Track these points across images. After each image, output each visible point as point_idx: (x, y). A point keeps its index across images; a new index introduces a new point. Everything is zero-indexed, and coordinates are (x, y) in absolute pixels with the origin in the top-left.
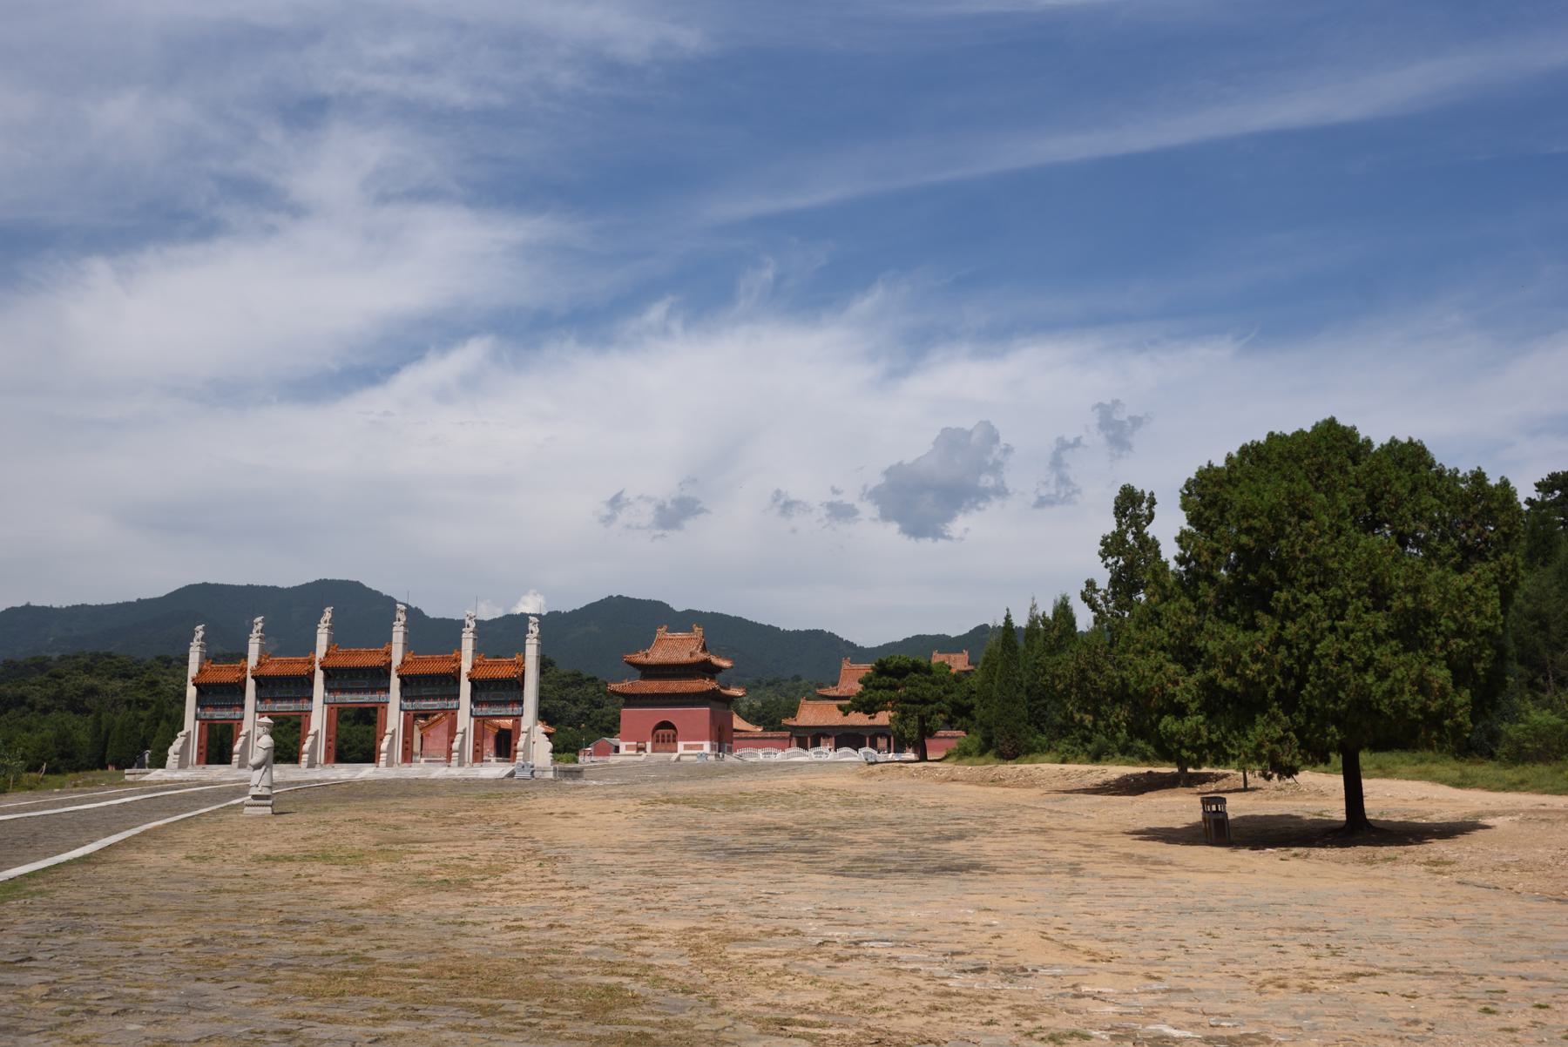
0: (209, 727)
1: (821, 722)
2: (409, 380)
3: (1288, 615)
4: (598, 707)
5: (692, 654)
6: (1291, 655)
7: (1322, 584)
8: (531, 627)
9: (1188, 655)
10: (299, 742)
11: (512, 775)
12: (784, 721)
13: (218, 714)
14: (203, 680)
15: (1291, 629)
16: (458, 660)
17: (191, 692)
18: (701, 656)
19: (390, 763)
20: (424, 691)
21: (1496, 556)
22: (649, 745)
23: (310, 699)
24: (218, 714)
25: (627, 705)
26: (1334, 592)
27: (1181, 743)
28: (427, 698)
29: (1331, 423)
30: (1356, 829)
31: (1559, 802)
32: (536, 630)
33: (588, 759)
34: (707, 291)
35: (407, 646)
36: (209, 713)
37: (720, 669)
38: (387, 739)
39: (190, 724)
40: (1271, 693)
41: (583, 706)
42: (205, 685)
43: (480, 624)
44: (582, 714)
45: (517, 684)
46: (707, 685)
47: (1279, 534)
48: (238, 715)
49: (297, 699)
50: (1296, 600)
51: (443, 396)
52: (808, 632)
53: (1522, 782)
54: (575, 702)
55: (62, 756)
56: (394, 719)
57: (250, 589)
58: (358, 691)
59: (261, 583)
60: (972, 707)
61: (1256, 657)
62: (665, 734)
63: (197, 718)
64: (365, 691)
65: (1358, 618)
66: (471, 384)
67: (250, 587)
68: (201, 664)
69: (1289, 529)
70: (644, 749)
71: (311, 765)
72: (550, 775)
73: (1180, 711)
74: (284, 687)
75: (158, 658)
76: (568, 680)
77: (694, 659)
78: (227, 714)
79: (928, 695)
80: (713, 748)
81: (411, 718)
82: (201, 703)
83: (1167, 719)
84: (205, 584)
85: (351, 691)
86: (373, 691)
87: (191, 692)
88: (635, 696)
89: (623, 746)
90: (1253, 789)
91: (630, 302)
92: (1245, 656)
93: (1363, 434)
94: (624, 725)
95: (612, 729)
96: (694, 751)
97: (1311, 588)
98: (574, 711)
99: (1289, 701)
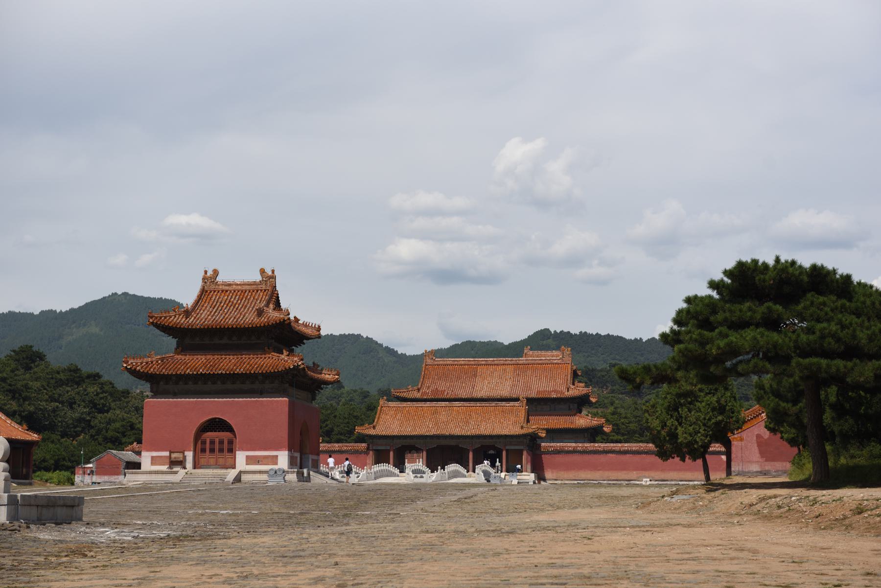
4: (101, 411)
5: (260, 313)
12: (358, 429)
22: (189, 455)
25: (156, 393)
33: (88, 479)
41: (81, 410)
44: (80, 420)
46: (285, 360)
52: (343, 337)
54: (71, 404)
62: (215, 440)
70: (181, 463)
76: (62, 376)
77: (264, 320)
80: (292, 462)
88: (167, 378)
89: (146, 459)
94: (148, 427)
95: (130, 435)
98: (71, 415)
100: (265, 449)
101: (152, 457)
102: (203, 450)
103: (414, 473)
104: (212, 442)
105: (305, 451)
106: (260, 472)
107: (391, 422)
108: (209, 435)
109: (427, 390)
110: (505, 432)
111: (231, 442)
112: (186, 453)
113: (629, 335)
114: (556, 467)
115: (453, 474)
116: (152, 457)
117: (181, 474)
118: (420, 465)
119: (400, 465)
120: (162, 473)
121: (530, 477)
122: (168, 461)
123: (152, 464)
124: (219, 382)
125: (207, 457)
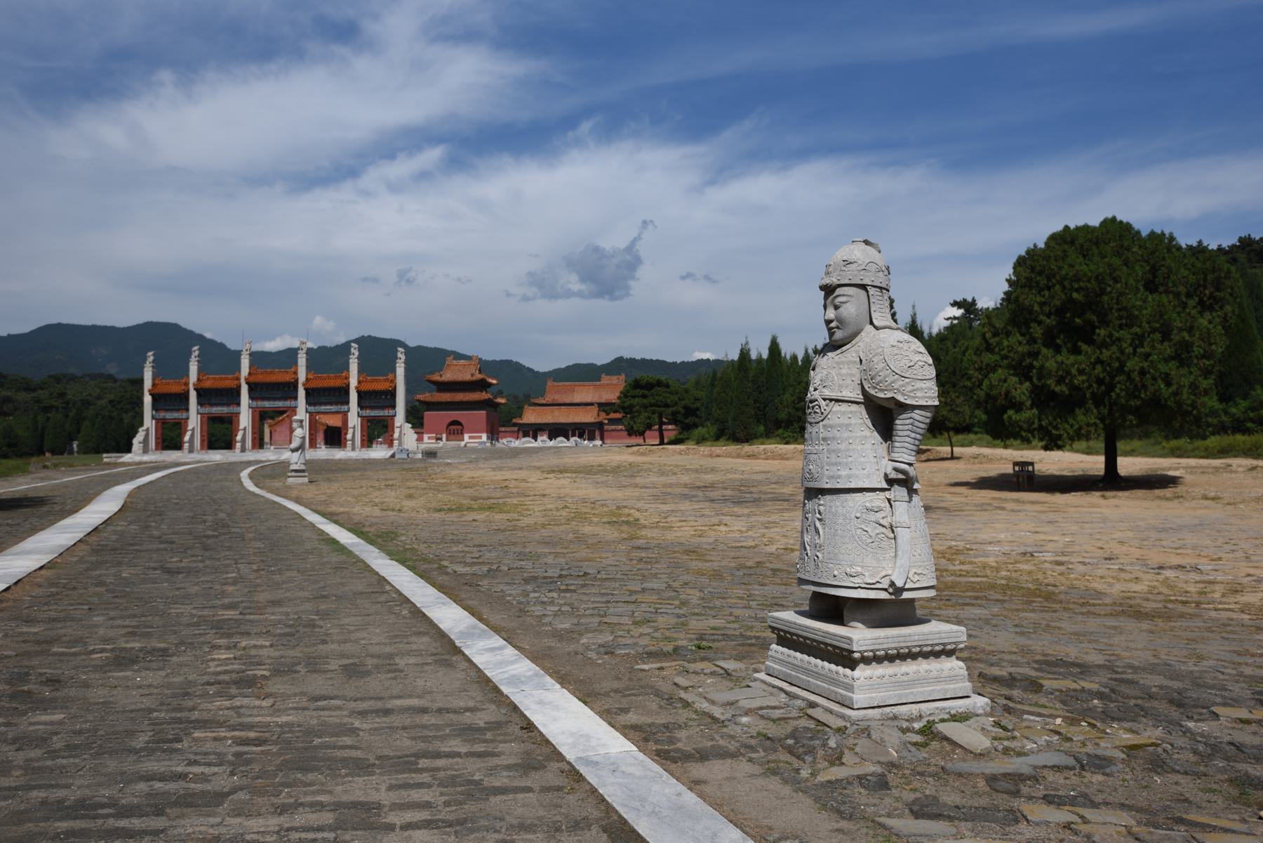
0: (162, 424)
1: (539, 421)
2: (373, 176)
3: (1104, 345)
6: (1104, 370)
7: (1127, 325)
8: (399, 355)
9: (1024, 372)
10: (181, 435)
11: (393, 456)
13: (169, 415)
14: (156, 391)
15: (1106, 354)
16: (347, 378)
17: (148, 399)
18: (478, 376)
19: (243, 450)
20: (322, 400)
21: (1221, 308)
22: (444, 436)
23: (239, 404)
24: (169, 415)
25: (428, 410)
26: (1136, 329)
27: (1021, 428)
28: (326, 404)
29: (1114, 219)
30: (1111, 481)
31: (1261, 463)
32: (403, 357)
34: (615, 121)
35: (309, 368)
36: (162, 415)
37: (490, 385)
38: (189, 433)
39: (149, 422)
40: (1088, 395)
42: (313, 390)
43: (309, 351)
45: (392, 394)
46: (484, 396)
47: (1103, 292)
48: (184, 415)
49: (228, 405)
50: (1110, 336)
51: (395, 188)
52: (502, 362)
53: (1133, 451)
55: (9, 446)
56: (245, 419)
57: (94, 329)
58: (275, 399)
59: (71, 322)
60: (697, 409)
61: (1081, 372)
62: (455, 429)
63: (153, 417)
64: (280, 399)
65: (1153, 347)
66: (423, 176)
67: (94, 327)
68: (154, 379)
69: (1109, 289)
71: (243, 450)
72: (420, 456)
73: (1018, 407)
74: (171, 400)
75: (50, 377)
78: (176, 415)
79: (669, 401)
81: (261, 417)
82: (155, 407)
83: (1010, 412)
84: (60, 324)
85: (269, 399)
86: (285, 399)
87: (148, 399)
90: (958, 458)
91: (569, 122)
92: (1074, 371)
93: (1136, 226)
96: (476, 440)
97: (1121, 326)
99: (1098, 401)
103: (543, 441)
105: (494, 435)
107: (531, 416)
109: (549, 398)
110: (587, 420)
113: (670, 360)
114: (611, 438)
115: (560, 442)
117: (441, 444)
118: (545, 438)
119: (535, 438)
121: (598, 442)
125: (452, 437)
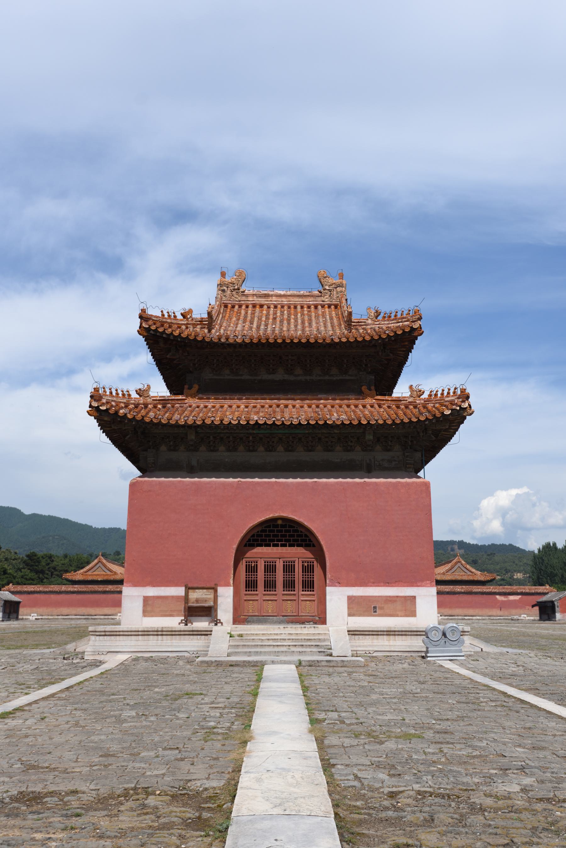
22: (226, 596)
52: (110, 529)
70: (209, 612)
100: (388, 583)
101: (146, 599)
102: (251, 585)
104: (270, 568)
106: (390, 633)
108: (261, 554)
111: (308, 569)
112: (220, 590)
116: (146, 599)
120: (172, 633)
122: (181, 606)
123: (146, 613)
124: (280, 448)
